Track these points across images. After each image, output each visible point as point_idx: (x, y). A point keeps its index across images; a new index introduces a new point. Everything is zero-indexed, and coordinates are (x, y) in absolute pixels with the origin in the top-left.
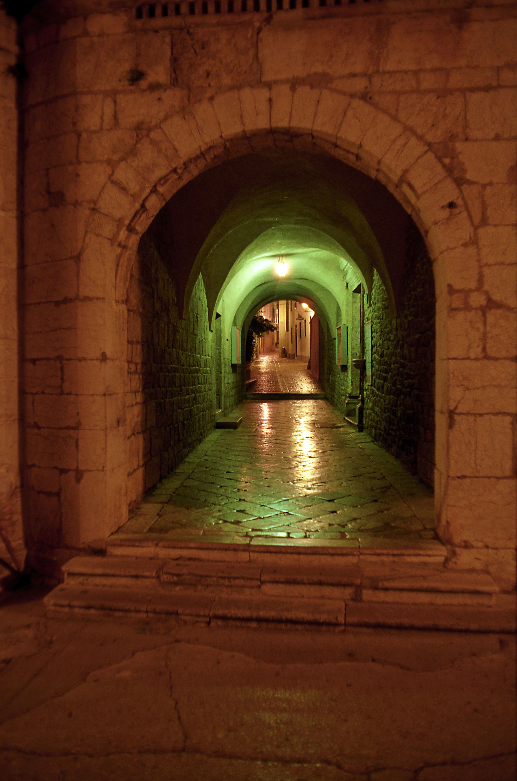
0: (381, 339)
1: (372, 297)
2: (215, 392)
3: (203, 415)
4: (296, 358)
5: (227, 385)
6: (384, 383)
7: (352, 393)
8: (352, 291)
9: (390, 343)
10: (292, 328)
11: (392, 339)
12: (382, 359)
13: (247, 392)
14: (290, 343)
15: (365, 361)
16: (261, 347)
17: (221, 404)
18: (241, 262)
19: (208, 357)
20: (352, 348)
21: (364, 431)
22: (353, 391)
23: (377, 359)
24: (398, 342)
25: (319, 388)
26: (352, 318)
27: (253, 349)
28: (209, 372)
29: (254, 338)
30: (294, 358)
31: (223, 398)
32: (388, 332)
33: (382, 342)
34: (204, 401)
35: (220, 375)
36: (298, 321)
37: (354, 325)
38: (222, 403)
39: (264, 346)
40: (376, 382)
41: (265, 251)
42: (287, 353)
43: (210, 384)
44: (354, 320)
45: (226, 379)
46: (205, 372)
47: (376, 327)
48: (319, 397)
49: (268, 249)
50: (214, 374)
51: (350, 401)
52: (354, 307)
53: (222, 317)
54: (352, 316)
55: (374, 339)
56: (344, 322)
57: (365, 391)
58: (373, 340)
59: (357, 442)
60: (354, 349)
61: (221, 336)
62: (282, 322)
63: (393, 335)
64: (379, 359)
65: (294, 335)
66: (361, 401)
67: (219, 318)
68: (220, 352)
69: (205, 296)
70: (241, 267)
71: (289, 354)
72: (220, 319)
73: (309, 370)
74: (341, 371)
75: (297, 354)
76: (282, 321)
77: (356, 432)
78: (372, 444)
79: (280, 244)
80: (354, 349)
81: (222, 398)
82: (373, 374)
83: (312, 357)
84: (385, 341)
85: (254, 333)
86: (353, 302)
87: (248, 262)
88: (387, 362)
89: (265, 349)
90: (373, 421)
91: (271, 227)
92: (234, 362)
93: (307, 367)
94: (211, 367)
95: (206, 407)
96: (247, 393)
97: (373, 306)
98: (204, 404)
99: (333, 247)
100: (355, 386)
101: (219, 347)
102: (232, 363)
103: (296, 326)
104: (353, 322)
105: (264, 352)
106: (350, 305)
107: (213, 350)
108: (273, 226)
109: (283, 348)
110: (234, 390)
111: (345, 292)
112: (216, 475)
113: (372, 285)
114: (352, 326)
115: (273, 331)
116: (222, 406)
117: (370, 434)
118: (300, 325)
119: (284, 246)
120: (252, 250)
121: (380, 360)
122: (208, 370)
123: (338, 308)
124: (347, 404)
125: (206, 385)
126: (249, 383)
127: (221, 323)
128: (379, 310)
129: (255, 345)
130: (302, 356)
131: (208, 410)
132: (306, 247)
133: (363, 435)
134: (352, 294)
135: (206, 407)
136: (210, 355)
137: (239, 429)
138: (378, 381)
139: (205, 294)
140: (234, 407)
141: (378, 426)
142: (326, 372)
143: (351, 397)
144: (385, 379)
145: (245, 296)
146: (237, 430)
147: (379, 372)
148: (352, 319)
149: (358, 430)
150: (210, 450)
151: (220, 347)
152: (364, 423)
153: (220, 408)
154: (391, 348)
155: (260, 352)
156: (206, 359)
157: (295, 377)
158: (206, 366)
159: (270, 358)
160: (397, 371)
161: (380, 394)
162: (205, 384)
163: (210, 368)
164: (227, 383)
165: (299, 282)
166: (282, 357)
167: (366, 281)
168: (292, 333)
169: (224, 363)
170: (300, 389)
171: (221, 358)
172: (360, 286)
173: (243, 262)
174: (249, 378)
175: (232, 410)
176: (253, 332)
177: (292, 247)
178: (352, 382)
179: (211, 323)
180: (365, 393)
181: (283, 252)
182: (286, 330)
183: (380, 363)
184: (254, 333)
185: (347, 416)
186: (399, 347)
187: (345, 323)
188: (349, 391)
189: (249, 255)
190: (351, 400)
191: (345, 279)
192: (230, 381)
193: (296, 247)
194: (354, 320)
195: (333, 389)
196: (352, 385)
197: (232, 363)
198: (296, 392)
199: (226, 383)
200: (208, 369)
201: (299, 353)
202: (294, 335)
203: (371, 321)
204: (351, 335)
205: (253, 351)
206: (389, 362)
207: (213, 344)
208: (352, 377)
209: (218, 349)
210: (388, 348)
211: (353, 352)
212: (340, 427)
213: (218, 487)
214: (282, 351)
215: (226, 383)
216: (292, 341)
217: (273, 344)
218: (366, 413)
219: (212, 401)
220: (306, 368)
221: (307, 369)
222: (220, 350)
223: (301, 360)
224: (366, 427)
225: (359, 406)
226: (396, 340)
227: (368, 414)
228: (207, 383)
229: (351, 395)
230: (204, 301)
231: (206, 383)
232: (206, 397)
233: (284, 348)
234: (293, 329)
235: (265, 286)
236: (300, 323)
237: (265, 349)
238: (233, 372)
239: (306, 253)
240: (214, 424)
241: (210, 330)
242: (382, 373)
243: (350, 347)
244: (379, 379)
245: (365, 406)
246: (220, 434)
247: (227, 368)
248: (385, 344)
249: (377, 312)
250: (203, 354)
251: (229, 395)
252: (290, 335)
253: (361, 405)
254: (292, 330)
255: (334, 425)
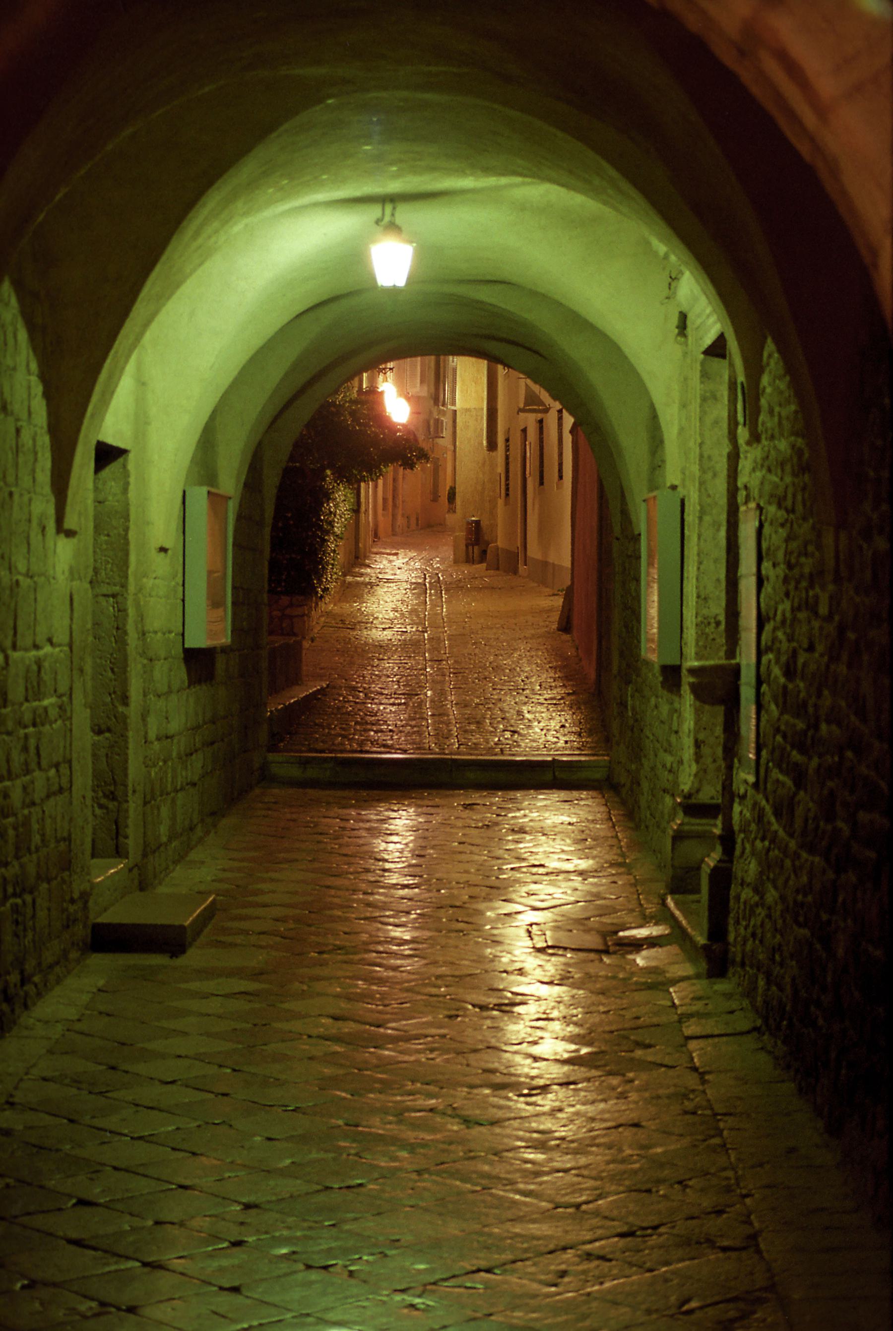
0: (787, 595)
1: (763, 402)
2: (90, 794)
3: (15, 909)
4: (522, 568)
5: (157, 746)
6: (795, 794)
7: (698, 791)
8: (703, 349)
9: (816, 624)
10: (507, 440)
11: (823, 610)
12: (790, 686)
13: (273, 748)
14: (501, 502)
15: (736, 671)
16: (380, 511)
17: (126, 837)
18: (209, 230)
19: (48, 649)
20: (698, 597)
21: (730, 974)
22: (700, 781)
23: (776, 677)
24: (842, 629)
25: (590, 732)
26: (701, 465)
27: (324, 541)
28: (53, 713)
29: (327, 496)
30: (515, 572)
31: (133, 806)
32: (811, 575)
33: (793, 610)
34: (22, 847)
35: (121, 709)
36: (530, 420)
37: (709, 496)
38: (130, 831)
39: (395, 506)
40: (770, 780)
41: (315, 183)
42: (488, 543)
43: (57, 766)
44: (710, 475)
45: (152, 720)
46: (28, 717)
47: (775, 537)
48: (584, 775)
49: (324, 177)
50: (82, 717)
51: (686, 828)
52: (709, 420)
53: (131, 456)
54: (701, 456)
55: (768, 588)
56: (672, 476)
57: (737, 800)
58: (763, 590)
59: (688, 1032)
60: (706, 599)
61: (127, 543)
62: (467, 410)
63: (827, 595)
64: (782, 680)
65: (515, 467)
66: (722, 844)
67: (121, 460)
68: (122, 611)
69: (38, 389)
70: (207, 254)
71: (497, 548)
72: (124, 466)
73: (566, 637)
74: (663, 684)
75: (529, 554)
76: (472, 404)
77: (698, 976)
78: (750, 1042)
79: (379, 158)
80: (706, 599)
81: (127, 811)
82: (761, 741)
83: (575, 580)
84: (799, 609)
85: (328, 472)
86: (704, 399)
87: (237, 228)
88: (805, 704)
89: (400, 521)
90: (761, 941)
91: (321, 101)
92: (198, 639)
93: (556, 616)
94: (63, 688)
95: (32, 869)
96: (271, 757)
97: (764, 442)
98: (24, 860)
99: (597, 181)
100: (710, 760)
101: (117, 589)
102: (186, 646)
103: (524, 431)
104: (702, 483)
105: (394, 534)
106: (695, 407)
107: (76, 615)
108: (329, 97)
109: (470, 523)
110: (198, 762)
111: (674, 349)
112: (25, 1220)
113: (761, 355)
114: (700, 497)
115: (412, 467)
116: (133, 842)
117: (750, 993)
118: (541, 429)
119: (392, 164)
120: (252, 185)
121: (785, 687)
122: (46, 709)
123: (654, 416)
124: (679, 837)
125: (37, 774)
126: (286, 708)
127: (127, 484)
128: (782, 465)
129: (331, 524)
130: (545, 564)
131: (49, 881)
132: (487, 170)
133: (724, 995)
134: (703, 364)
135: (32, 869)
136: (61, 637)
137: (194, 957)
138: (776, 774)
139: (34, 379)
140: (199, 831)
141: (776, 970)
142: (615, 669)
143: (694, 809)
144: (799, 776)
145: (240, 358)
146: (181, 961)
147: (779, 738)
148: (703, 470)
149: (704, 966)
150: (35, 1072)
151: (124, 586)
152: (731, 937)
153: (119, 852)
154: (820, 648)
155: (376, 535)
156: (39, 663)
157: (497, 669)
158: (35, 691)
159: (418, 565)
160: (836, 759)
161: (781, 833)
162: (28, 772)
163: (60, 696)
164: (158, 739)
165: (485, 295)
166: (469, 560)
167: (736, 332)
168: (507, 457)
169: (143, 654)
170: (508, 735)
171: (126, 633)
172: (721, 340)
173: (216, 232)
174: (295, 679)
175: (190, 848)
176: (323, 469)
177: (432, 169)
178: (698, 744)
179: (66, 496)
180: (737, 808)
181: (394, 186)
182: (485, 443)
183: (784, 697)
184: (328, 472)
185: (673, 892)
186: (845, 657)
187: (676, 483)
188: (686, 783)
189: (239, 204)
190: (693, 821)
191: (675, 293)
192: (174, 726)
193: (450, 172)
194: (710, 475)
195: (637, 752)
196: (698, 757)
197: (186, 646)
198: (490, 750)
199: (152, 735)
200: (46, 702)
201: (534, 551)
202: (515, 467)
203: (758, 506)
204: (695, 538)
205: (324, 553)
206: (811, 710)
207: (82, 587)
208: (696, 724)
209: (114, 596)
210: (811, 648)
211: (705, 612)
212: (637, 945)
213: (19, 1285)
214: (469, 531)
215: (152, 735)
216: (507, 495)
217: (435, 498)
218: (738, 898)
219: (68, 839)
220: (555, 626)
221: (559, 629)
222: (120, 599)
223: (544, 583)
224: (738, 959)
225: (712, 864)
226: (837, 618)
227: (745, 903)
228: (44, 763)
229: (693, 801)
230: (30, 413)
231: (33, 765)
232: (35, 827)
233: (478, 523)
234: (511, 443)
235: (327, 316)
236: (541, 422)
237: (400, 521)
238: (191, 683)
239: (498, 188)
240: (80, 931)
241: (60, 528)
242: (789, 748)
243: (690, 588)
244: (781, 771)
245: (738, 868)
246: (101, 983)
247: (160, 671)
248: (800, 621)
249: (776, 475)
250: (19, 643)
251: (169, 788)
252: (500, 469)
253: (720, 861)
254: (507, 448)
255: (616, 932)
